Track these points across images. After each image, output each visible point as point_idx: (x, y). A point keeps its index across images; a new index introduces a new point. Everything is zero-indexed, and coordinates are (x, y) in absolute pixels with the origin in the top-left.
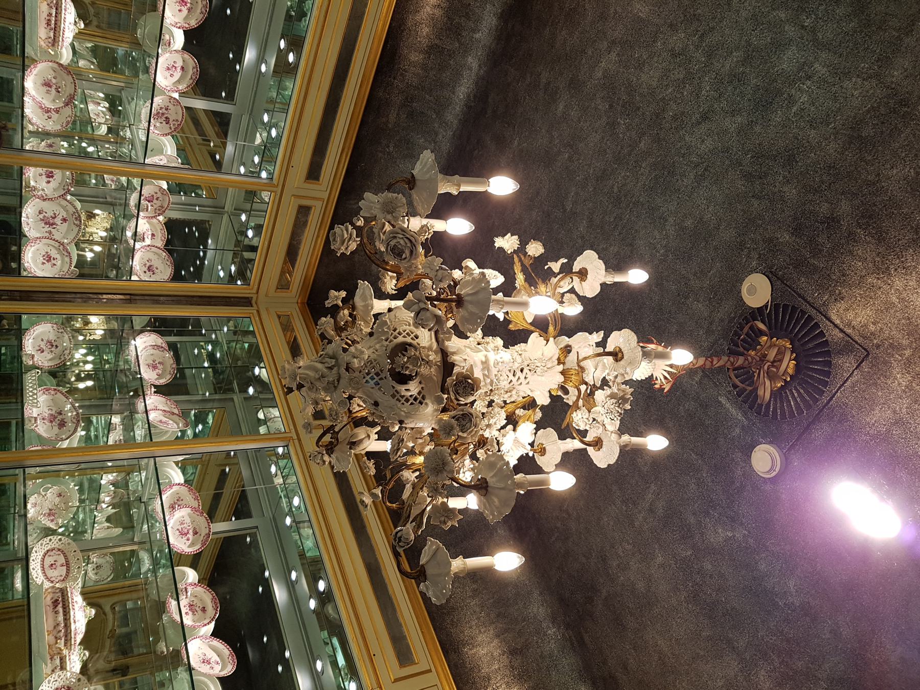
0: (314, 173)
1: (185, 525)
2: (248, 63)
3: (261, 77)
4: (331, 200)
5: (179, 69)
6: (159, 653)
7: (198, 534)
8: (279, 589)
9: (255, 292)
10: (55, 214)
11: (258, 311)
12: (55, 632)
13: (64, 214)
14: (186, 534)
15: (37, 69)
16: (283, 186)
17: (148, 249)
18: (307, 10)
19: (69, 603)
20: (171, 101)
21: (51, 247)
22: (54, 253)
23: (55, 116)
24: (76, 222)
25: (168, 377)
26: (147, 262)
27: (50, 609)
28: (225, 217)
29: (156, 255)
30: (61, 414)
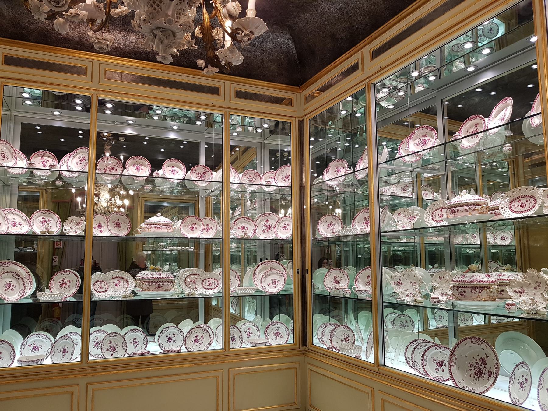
0: (215, 91)
1: (420, 142)
2: (178, 137)
3: (180, 129)
4: (229, 79)
5: (173, 169)
6: (510, 152)
7: (426, 134)
8: (482, 79)
9: (295, 119)
10: (264, 225)
11: (306, 115)
12: (470, 211)
13: (264, 222)
14: (425, 141)
15: (185, 233)
16: (225, 108)
17: (276, 179)
18: (183, 114)
19: (457, 204)
20: (193, 172)
21: (280, 226)
22: (282, 225)
23: (210, 226)
24: (268, 215)
25: (344, 162)
26: (284, 179)
27: (456, 214)
28: (266, 142)
29: (280, 175)
30: (366, 218)
